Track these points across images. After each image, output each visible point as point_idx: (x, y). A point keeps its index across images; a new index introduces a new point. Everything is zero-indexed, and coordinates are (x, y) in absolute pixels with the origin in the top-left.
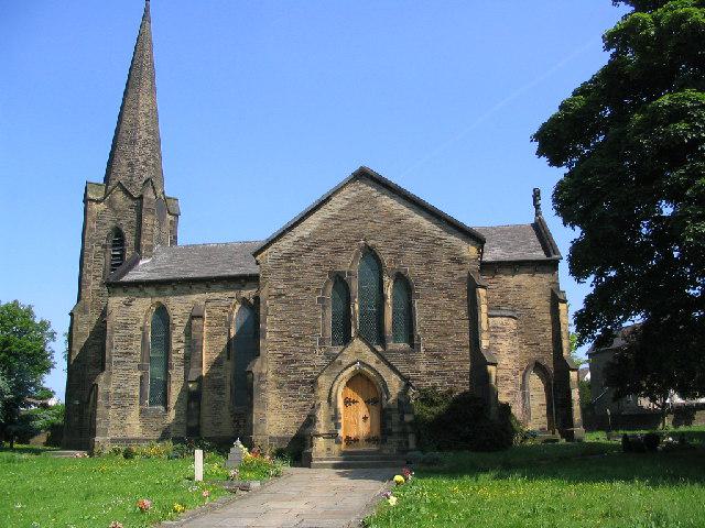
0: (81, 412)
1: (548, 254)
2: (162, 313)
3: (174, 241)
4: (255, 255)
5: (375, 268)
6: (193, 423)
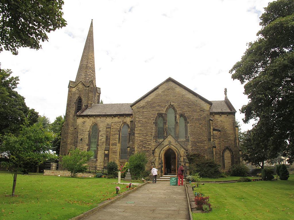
2: (95, 127)
3: (98, 102)
4: (131, 106)
5: (170, 103)
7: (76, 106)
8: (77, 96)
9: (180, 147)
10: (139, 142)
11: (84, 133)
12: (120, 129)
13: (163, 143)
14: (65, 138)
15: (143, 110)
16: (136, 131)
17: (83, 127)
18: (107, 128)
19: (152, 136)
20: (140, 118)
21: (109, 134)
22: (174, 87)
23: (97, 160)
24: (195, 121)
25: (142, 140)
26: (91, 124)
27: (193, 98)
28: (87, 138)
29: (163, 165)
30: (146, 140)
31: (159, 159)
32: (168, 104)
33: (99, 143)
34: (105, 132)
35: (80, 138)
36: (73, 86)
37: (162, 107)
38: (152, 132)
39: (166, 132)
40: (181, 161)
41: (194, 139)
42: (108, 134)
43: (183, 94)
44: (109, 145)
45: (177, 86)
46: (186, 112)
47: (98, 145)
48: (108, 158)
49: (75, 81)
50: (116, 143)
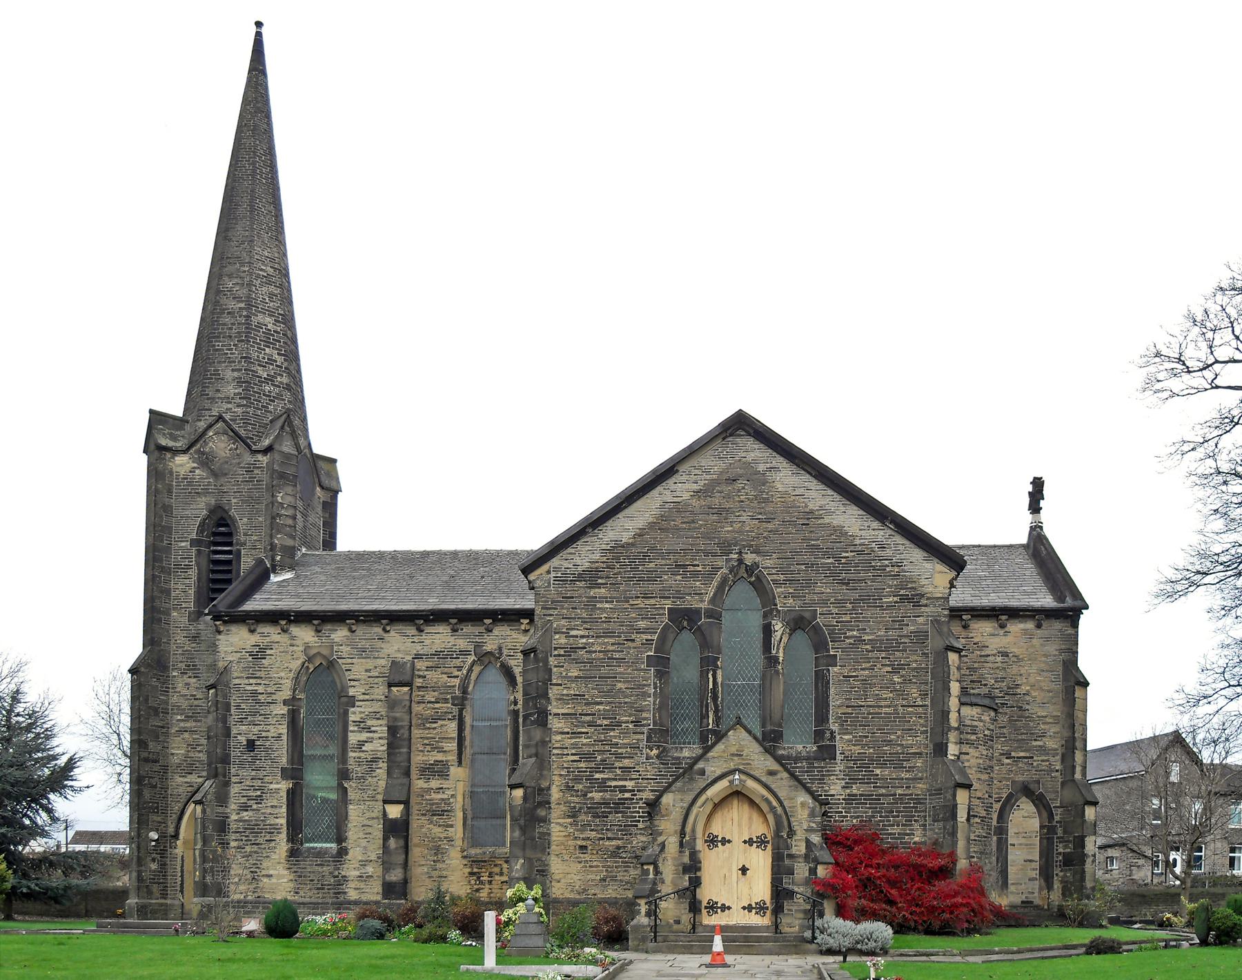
0: (163, 853)
1: (1061, 599)
2: (321, 676)
3: (330, 542)
4: (526, 571)
6: (396, 876)
7: (204, 562)
13: (700, 765)
17: (252, 681)
20: (573, 633)
22: (761, 468)
23: (342, 852)
25: (586, 749)
26: (299, 662)
28: (285, 737)
30: (607, 748)
31: (681, 845)
33: (351, 761)
35: (243, 739)
37: (695, 575)
40: (791, 856)
42: (398, 715)
46: (824, 602)
48: (402, 842)
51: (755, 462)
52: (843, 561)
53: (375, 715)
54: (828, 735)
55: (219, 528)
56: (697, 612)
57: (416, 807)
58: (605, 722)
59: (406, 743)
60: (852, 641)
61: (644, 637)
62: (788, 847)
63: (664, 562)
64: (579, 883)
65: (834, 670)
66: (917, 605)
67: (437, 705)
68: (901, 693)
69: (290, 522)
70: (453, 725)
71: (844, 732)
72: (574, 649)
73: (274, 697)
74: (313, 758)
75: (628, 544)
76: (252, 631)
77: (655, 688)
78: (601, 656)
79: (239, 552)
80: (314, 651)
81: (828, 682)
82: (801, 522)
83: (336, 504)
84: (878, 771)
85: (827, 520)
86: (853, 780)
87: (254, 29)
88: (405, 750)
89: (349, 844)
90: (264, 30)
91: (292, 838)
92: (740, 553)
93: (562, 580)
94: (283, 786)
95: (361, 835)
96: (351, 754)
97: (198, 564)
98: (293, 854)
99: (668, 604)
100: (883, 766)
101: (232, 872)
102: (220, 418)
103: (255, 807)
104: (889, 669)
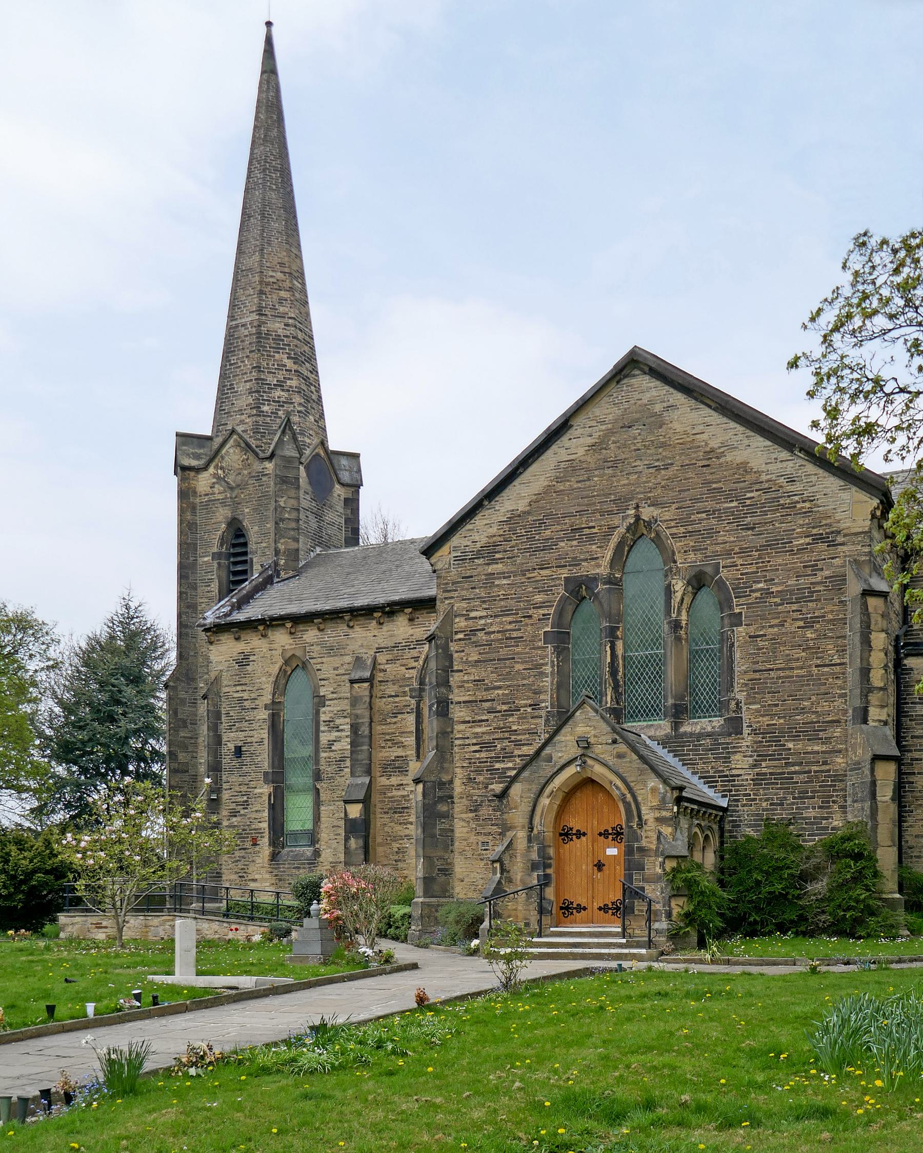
3: (353, 535)
7: (224, 574)
8: (222, 515)
9: (642, 772)
10: (477, 748)
11: (250, 715)
12: (422, 683)
13: (547, 751)
14: (185, 748)
15: (491, 569)
16: (456, 691)
17: (239, 688)
18: (352, 682)
19: (536, 713)
20: (473, 614)
21: (367, 714)
22: (658, 408)
23: (317, 853)
24: (777, 605)
25: (487, 738)
26: (277, 666)
27: (770, 467)
28: (266, 742)
29: (549, 871)
30: (507, 735)
31: (530, 840)
32: (624, 518)
33: (322, 761)
34: (345, 705)
35: (231, 746)
36: (194, 463)
37: (591, 538)
38: (537, 692)
39: (616, 687)
40: (641, 850)
41: (772, 716)
42: (359, 712)
43: (714, 444)
44: (369, 772)
45: (678, 398)
46: (728, 553)
47: (317, 776)
48: (361, 842)
49: (210, 434)
50: (404, 759)
51: (652, 402)
52: (748, 502)
53: (341, 714)
54: (733, 705)
55: (237, 536)
56: (595, 579)
57: (379, 805)
58: (505, 707)
59: (367, 740)
60: (758, 594)
61: (541, 612)
62: (637, 839)
63: (559, 527)
64: (481, 882)
65: (741, 631)
66: (833, 544)
67: (397, 699)
68: (814, 650)
69: (293, 525)
70: (412, 718)
71: (750, 700)
72: (474, 632)
73: (257, 702)
74: (294, 760)
75: (524, 513)
76: (238, 639)
77: (553, 666)
78: (500, 636)
79: (251, 559)
80: (288, 655)
81: (733, 645)
82: (701, 463)
83: (357, 500)
84: (790, 745)
85: (729, 458)
86: (763, 757)
87: (264, 29)
88: (366, 747)
89: (322, 846)
90: (274, 29)
91: (274, 843)
92: (637, 507)
93: (461, 560)
94: (265, 790)
95: (333, 837)
96: (323, 755)
97: (219, 577)
98: (274, 857)
99: (564, 573)
100: (795, 738)
101: (224, 878)
102: (233, 431)
103: (242, 812)
104: (801, 624)
